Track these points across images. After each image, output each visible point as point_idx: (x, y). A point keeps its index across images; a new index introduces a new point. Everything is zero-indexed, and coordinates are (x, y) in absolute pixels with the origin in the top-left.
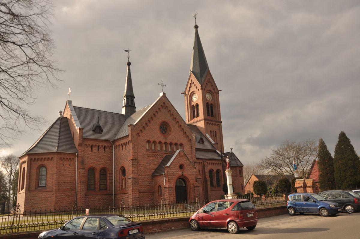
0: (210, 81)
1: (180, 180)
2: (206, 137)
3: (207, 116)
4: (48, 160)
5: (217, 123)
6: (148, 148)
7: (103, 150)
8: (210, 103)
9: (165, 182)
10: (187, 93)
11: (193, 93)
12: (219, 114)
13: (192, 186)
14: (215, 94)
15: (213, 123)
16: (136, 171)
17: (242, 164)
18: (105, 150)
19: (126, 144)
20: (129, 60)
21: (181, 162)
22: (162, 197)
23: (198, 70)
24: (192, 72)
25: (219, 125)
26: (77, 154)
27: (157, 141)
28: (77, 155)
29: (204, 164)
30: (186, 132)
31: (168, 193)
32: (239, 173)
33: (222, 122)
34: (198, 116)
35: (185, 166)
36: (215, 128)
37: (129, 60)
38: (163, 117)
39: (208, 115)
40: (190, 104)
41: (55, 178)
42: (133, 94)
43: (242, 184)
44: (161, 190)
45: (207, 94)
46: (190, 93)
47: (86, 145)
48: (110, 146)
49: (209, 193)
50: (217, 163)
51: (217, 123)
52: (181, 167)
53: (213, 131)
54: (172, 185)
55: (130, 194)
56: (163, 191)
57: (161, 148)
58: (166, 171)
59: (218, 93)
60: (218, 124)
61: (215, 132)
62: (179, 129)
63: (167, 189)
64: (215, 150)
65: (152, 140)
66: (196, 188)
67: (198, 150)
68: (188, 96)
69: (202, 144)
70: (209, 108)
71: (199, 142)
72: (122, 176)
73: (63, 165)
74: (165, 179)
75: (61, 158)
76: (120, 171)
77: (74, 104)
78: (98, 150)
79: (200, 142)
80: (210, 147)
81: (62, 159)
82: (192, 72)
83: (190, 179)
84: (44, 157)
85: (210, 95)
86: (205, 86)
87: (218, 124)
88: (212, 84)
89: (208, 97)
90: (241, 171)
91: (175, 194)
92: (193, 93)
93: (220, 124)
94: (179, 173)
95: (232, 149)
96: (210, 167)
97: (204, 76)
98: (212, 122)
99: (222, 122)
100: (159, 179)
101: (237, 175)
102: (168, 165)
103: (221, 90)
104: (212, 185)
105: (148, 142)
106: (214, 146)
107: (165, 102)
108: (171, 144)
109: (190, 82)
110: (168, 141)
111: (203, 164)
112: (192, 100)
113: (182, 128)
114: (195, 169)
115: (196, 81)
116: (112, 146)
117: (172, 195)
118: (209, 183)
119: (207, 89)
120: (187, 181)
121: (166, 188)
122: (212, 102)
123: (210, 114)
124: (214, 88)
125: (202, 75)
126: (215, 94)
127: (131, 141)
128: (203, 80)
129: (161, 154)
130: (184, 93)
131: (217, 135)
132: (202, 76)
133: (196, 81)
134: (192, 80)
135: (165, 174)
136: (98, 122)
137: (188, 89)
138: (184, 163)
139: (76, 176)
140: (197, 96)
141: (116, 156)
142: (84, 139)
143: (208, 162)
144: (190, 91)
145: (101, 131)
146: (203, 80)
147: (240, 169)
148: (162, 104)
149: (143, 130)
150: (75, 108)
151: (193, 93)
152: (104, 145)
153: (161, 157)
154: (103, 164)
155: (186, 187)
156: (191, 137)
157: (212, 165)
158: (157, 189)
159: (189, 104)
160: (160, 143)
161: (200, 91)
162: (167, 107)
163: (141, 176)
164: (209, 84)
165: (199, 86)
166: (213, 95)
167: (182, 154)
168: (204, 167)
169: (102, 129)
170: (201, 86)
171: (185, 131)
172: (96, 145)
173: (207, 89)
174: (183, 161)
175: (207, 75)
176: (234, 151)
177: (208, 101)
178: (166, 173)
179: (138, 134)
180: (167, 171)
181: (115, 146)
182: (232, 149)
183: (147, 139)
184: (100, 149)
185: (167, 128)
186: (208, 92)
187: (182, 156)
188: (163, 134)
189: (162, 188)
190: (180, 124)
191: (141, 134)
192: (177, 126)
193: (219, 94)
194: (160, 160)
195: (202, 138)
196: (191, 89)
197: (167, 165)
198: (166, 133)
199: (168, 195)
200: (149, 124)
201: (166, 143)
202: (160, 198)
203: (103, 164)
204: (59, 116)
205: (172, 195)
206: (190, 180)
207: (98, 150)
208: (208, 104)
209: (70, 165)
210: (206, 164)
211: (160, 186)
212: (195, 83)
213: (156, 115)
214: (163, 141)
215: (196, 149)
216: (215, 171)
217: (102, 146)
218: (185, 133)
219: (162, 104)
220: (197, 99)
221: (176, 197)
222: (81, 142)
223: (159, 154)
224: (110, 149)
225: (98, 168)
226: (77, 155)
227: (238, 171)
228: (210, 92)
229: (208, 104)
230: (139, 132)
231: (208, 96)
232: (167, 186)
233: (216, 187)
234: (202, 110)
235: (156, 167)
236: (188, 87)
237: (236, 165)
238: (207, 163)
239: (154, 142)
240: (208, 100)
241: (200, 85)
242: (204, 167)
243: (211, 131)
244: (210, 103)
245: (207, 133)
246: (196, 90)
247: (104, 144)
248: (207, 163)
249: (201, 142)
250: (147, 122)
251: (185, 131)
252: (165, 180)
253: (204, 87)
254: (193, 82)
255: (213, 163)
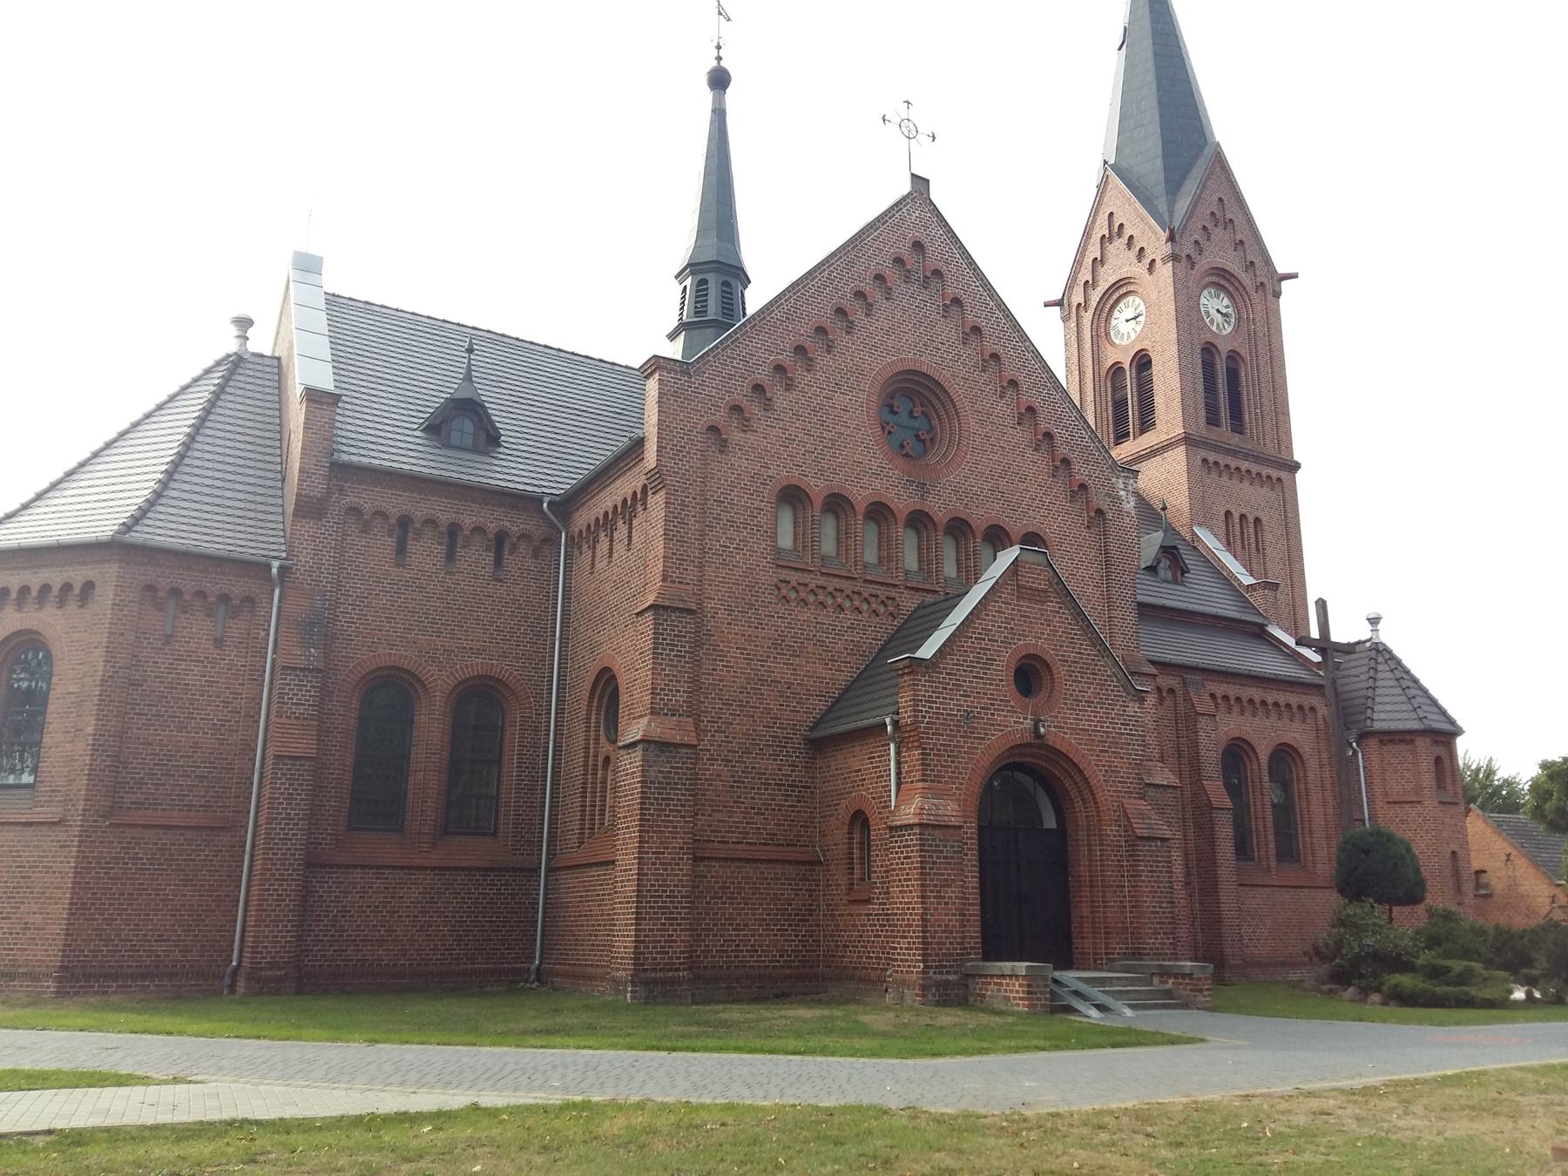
0: (1228, 216)
1: (1020, 776)
2: (1194, 545)
3: (1202, 421)
4: (62, 603)
5: (1265, 471)
6: (786, 540)
7: (489, 558)
8: (1224, 348)
9: (899, 785)
10: (1078, 297)
11: (1124, 290)
12: (1281, 416)
13: (1110, 830)
14: (1256, 297)
15: (1245, 465)
16: (682, 697)
17: (1452, 722)
18: (498, 562)
19: (629, 509)
20: (719, 58)
21: (1037, 641)
22: (868, 901)
23: (1152, 168)
24: (1114, 167)
25: (1279, 479)
26: (281, 568)
27: (861, 496)
28: (274, 571)
29: (1187, 699)
30: (1073, 456)
31: (915, 874)
32: (1428, 779)
33: (1297, 466)
34: (1146, 422)
35: (1061, 671)
36: (1251, 498)
37: (719, 58)
38: (902, 336)
39: (1213, 420)
40: (1097, 361)
41: (90, 729)
42: (736, 253)
43: (1454, 853)
44: (865, 844)
45: (1205, 293)
46: (1095, 297)
47: (355, 511)
48: (538, 533)
49: (1223, 899)
50: (1276, 704)
51: (1265, 471)
52: (1030, 675)
53: (1243, 517)
54: (950, 810)
55: (627, 859)
56: (878, 860)
57: (888, 555)
58: (905, 699)
59: (1277, 294)
60: (1275, 474)
61: (1257, 521)
62: (1020, 436)
63: (912, 838)
64: (1262, 626)
65: (818, 487)
66: (1144, 847)
67: (1150, 613)
68: (1087, 317)
69: (1175, 581)
70: (1215, 383)
71: (1152, 569)
72: (603, 739)
73: (168, 639)
74: (898, 763)
75: (150, 588)
76: (590, 705)
77: (334, 281)
78: (450, 557)
79: (1162, 573)
80: (1225, 607)
81: (161, 594)
82: (1114, 167)
83: (1097, 777)
84: (35, 579)
85: (1226, 302)
86: (1196, 242)
87: (1275, 474)
88: (1238, 237)
89: (1213, 312)
90: (1447, 764)
91: (973, 881)
92: (1120, 289)
93: (1283, 475)
94: (1012, 722)
95: (1374, 621)
96: (1232, 725)
97: (1190, 187)
98: (1233, 463)
99: (1297, 466)
100: (854, 763)
101: (1418, 790)
102: (927, 650)
103: (1294, 276)
104: (1242, 848)
105: (792, 496)
106: (1256, 599)
107: (926, 241)
108: (958, 528)
109: (1101, 229)
110: (940, 508)
111: (1180, 700)
112: (1107, 334)
113: (1043, 426)
114: (1133, 708)
115: (1136, 209)
116: (551, 541)
117: (951, 893)
118: (1225, 830)
119: (1204, 263)
120: (1074, 793)
121: (901, 827)
122: (1235, 345)
123: (1224, 413)
124: (1250, 258)
125: (1174, 181)
126: (1256, 297)
127: (658, 479)
128: (1183, 204)
129: (882, 592)
130: (1059, 303)
131: (1271, 533)
132: (1173, 185)
133: (1136, 209)
134: (1111, 214)
135: (895, 724)
136: (468, 377)
137: (1085, 275)
138: (1049, 654)
139: (258, 722)
140: (1142, 308)
141: (574, 606)
142: (344, 473)
143: (1220, 689)
144: (1094, 284)
145: (482, 438)
146: (1183, 204)
147: (1441, 751)
148: (905, 251)
149: (756, 410)
150: (333, 300)
151: (1124, 290)
152: (492, 528)
153: (882, 609)
154: (478, 653)
155: (1061, 833)
156: (1110, 496)
157: (1242, 713)
158: (840, 835)
159: (1088, 345)
160: (879, 512)
161: (1165, 271)
162: (938, 273)
163: (719, 737)
164: (1218, 233)
165: (1156, 243)
166: (1241, 304)
167: (1036, 579)
168: (1185, 722)
169: (492, 423)
170: (1171, 238)
171: (1063, 450)
172: (431, 522)
173: (1204, 263)
174: (1046, 634)
175: (1208, 178)
176: (1387, 636)
177: (1209, 337)
178: (906, 718)
179: (714, 429)
180: (916, 702)
181: (571, 540)
182: (1374, 621)
183: (783, 474)
184: (460, 552)
185: (936, 422)
186: (1213, 279)
187: (1038, 596)
188: (906, 455)
189: (877, 831)
190: (1025, 400)
191: (736, 436)
192: (1004, 409)
193: (1285, 302)
194: (875, 631)
195: (1175, 548)
196: (1101, 271)
197: (918, 654)
198: (925, 451)
199: (915, 899)
200: (801, 377)
201: (919, 521)
202: (855, 909)
203: (478, 653)
204: (232, 346)
205: (951, 893)
206: (1093, 782)
207: (450, 557)
208: (1209, 350)
209: (219, 642)
210: (1203, 704)
211: (860, 820)
212: (1127, 232)
213: (858, 316)
214: (902, 501)
215: (1141, 605)
216: (1264, 756)
217: (478, 530)
218: (1066, 462)
219: (905, 251)
220: (1138, 329)
221: (983, 904)
222: (318, 488)
223: (869, 590)
224: (535, 556)
225: (440, 680)
226: (274, 571)
227: (1426, 764)
228: (1222, 280)
229: (1209, 350)
230: (720, 417)
231: (1214, 305)
232: (909, 812)
233: (1273, 863)
234: (1175, 381)
235: (844, 678)
236: (1088, 261)
237: (1416, 725)
238: (1213, 696)
239: (837, 504)
240: (1214, 328)
241: (1164, 236)
242: (1185, 722)
243: (1228, 514)
244: (1224, 348)
245: (1200, 525)
246: (1139, 270)
247: (495, 520)
248: (1213, 696)
249: (1164, 572)
250: (786, 358)
251: (1063, 450)
252: (898, 774)
253: (1188, 249)
254: (1121, 225)
255: (1251, 701)
